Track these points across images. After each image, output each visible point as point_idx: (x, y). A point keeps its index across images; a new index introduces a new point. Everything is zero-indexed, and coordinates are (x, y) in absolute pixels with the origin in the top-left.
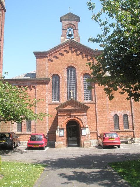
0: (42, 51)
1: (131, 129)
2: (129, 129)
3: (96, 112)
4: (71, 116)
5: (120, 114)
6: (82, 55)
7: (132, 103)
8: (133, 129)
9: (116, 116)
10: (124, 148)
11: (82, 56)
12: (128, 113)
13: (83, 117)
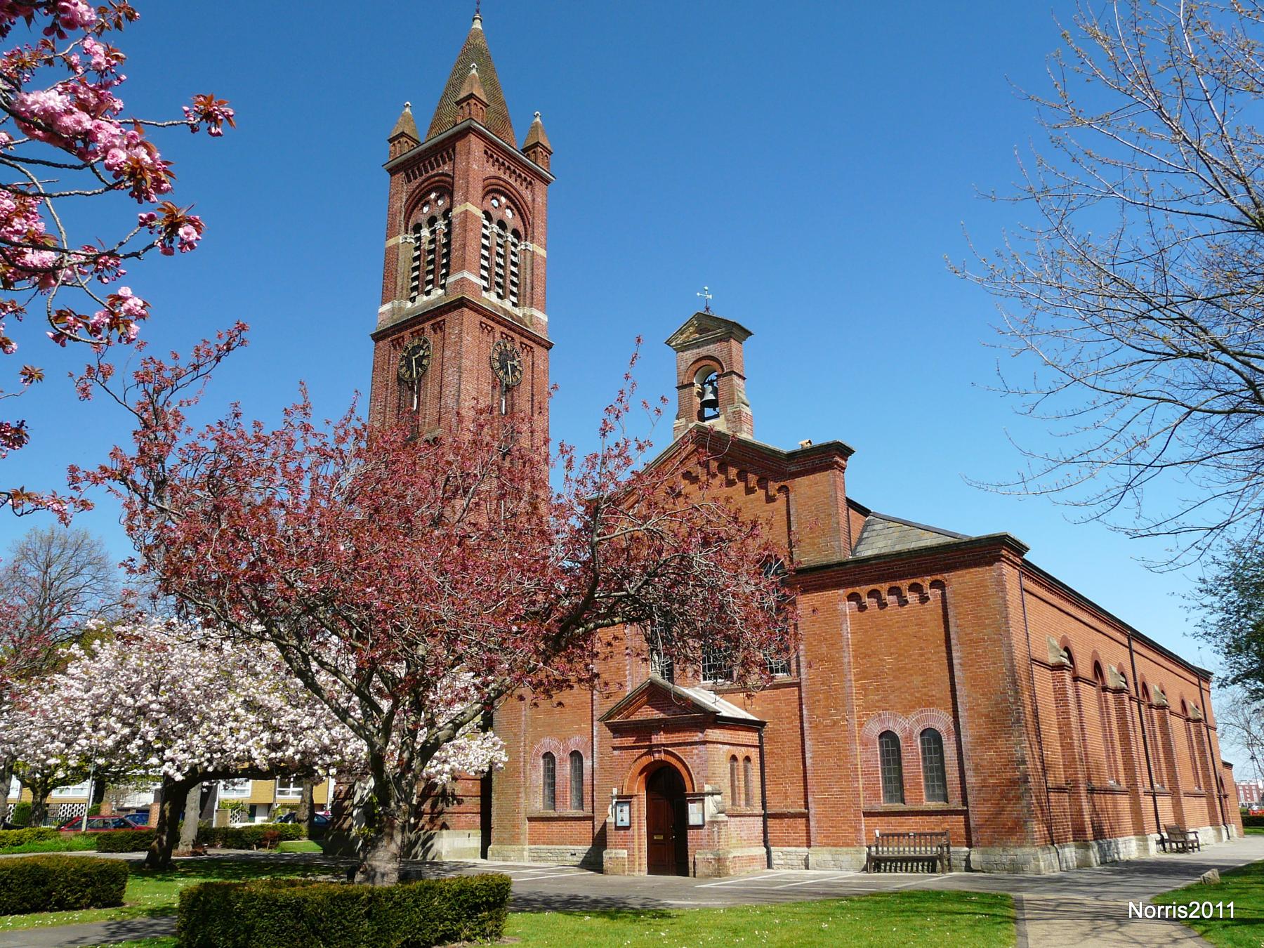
0: (770, 446)
1: (956, 803)
2: (903, 801)
3: (802, 723)
4: (651, 750)
5: (907, 726)
6: (746, 481)
7: (956, 673)
8: (965, 802)
9: (888, 737)
10: (1079, 897)
11: (746, 486)
12: (941, 721)
13: (695, 751)
